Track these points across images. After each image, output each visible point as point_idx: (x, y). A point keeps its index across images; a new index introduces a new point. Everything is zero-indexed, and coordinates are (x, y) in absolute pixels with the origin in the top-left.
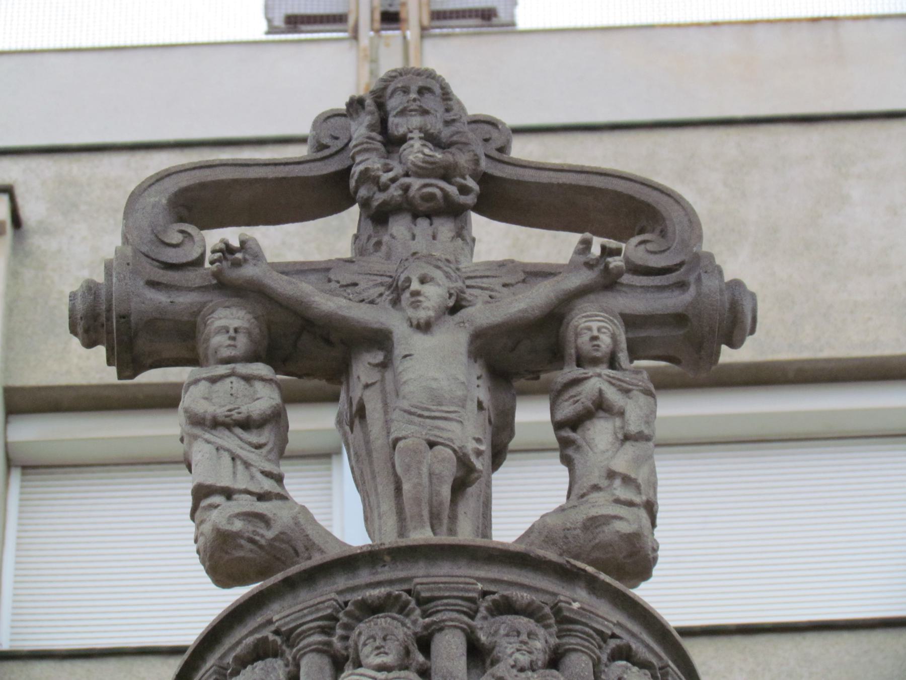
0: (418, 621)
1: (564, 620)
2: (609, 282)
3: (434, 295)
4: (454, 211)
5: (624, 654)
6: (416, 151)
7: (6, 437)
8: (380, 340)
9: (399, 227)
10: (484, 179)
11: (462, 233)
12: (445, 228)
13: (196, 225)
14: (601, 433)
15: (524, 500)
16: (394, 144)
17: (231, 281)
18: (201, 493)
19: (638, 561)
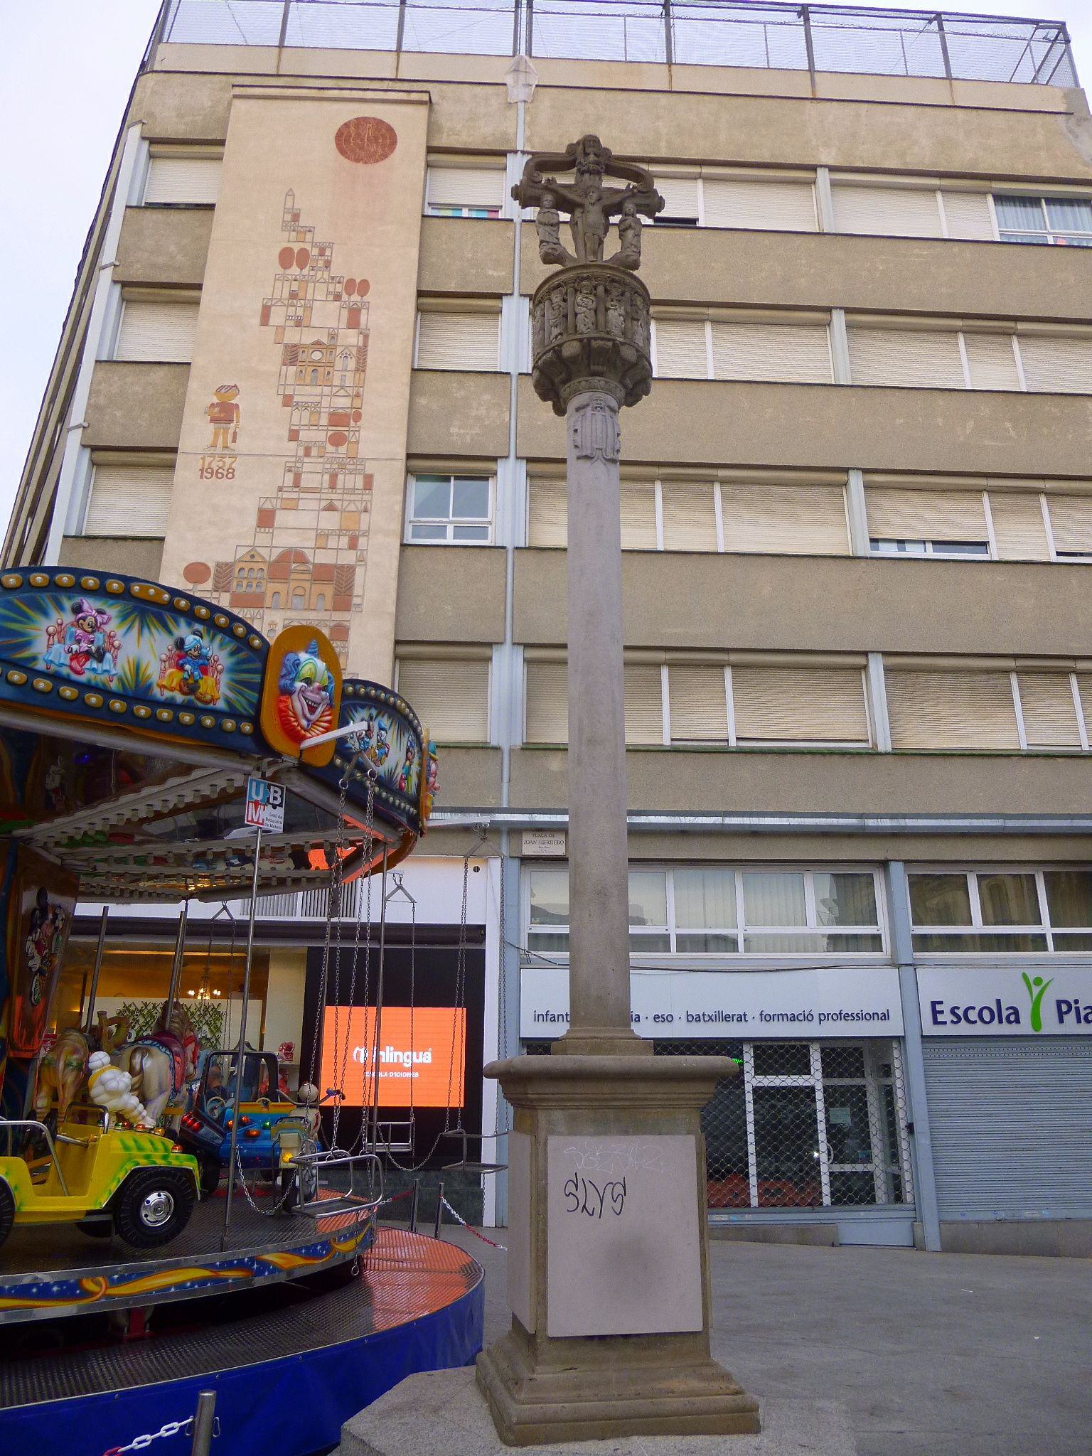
0: (594, 283)
1: (625, 284)
2: (634, 195)
3: (595, 196)
4: (599, 173)
5: (636, 292)
6: (592, 157)
7: (821, 166)
8: (581, 206)
9: (587, 176)
10: (607, 166)
11: (601, 180)
12: (597, 178)
13: (418, 1368)
14: (630, 233)
15: (612, 247)
16: (586, 154)
17: (550, 187)
18: (542, 242)
19: (636, 266)
